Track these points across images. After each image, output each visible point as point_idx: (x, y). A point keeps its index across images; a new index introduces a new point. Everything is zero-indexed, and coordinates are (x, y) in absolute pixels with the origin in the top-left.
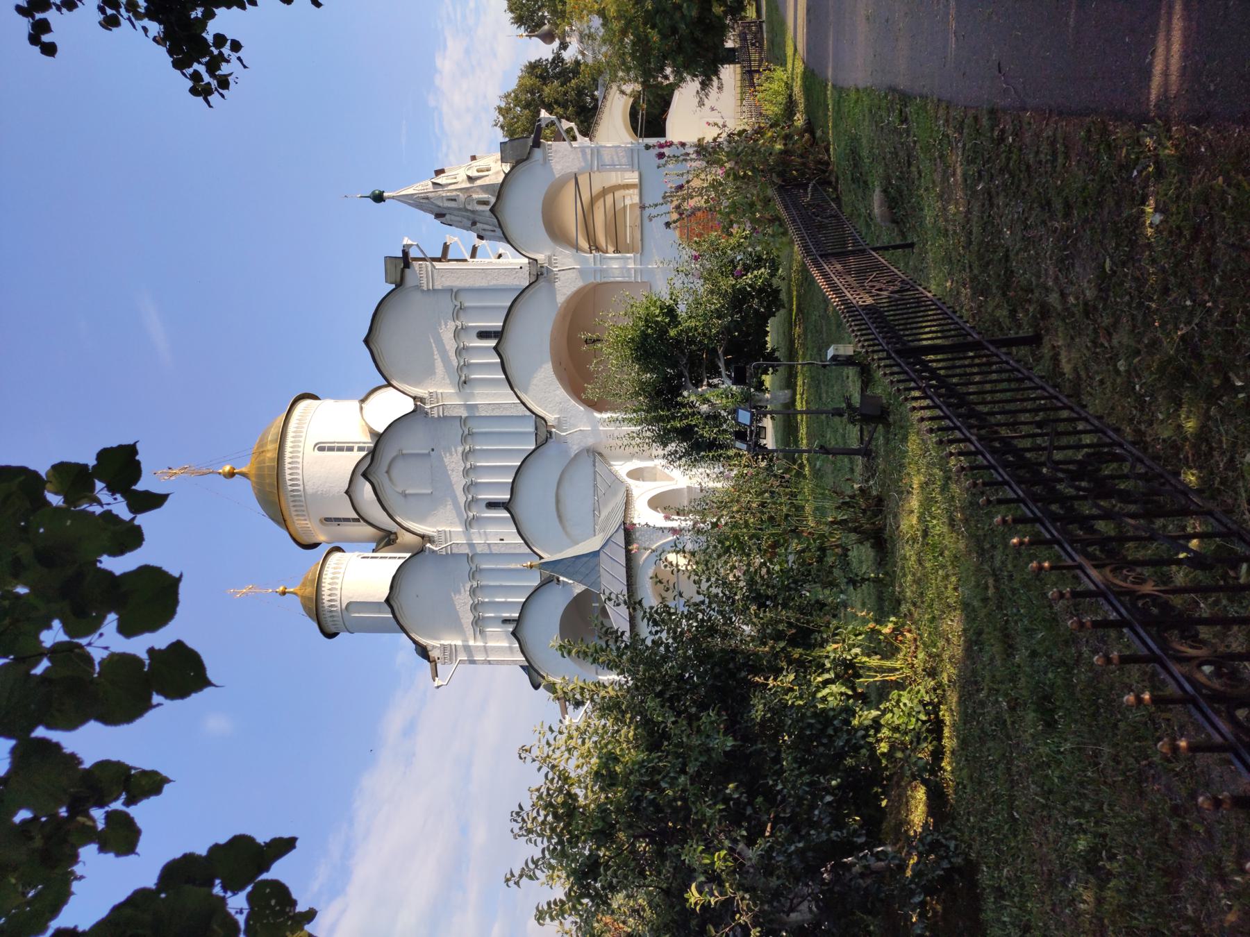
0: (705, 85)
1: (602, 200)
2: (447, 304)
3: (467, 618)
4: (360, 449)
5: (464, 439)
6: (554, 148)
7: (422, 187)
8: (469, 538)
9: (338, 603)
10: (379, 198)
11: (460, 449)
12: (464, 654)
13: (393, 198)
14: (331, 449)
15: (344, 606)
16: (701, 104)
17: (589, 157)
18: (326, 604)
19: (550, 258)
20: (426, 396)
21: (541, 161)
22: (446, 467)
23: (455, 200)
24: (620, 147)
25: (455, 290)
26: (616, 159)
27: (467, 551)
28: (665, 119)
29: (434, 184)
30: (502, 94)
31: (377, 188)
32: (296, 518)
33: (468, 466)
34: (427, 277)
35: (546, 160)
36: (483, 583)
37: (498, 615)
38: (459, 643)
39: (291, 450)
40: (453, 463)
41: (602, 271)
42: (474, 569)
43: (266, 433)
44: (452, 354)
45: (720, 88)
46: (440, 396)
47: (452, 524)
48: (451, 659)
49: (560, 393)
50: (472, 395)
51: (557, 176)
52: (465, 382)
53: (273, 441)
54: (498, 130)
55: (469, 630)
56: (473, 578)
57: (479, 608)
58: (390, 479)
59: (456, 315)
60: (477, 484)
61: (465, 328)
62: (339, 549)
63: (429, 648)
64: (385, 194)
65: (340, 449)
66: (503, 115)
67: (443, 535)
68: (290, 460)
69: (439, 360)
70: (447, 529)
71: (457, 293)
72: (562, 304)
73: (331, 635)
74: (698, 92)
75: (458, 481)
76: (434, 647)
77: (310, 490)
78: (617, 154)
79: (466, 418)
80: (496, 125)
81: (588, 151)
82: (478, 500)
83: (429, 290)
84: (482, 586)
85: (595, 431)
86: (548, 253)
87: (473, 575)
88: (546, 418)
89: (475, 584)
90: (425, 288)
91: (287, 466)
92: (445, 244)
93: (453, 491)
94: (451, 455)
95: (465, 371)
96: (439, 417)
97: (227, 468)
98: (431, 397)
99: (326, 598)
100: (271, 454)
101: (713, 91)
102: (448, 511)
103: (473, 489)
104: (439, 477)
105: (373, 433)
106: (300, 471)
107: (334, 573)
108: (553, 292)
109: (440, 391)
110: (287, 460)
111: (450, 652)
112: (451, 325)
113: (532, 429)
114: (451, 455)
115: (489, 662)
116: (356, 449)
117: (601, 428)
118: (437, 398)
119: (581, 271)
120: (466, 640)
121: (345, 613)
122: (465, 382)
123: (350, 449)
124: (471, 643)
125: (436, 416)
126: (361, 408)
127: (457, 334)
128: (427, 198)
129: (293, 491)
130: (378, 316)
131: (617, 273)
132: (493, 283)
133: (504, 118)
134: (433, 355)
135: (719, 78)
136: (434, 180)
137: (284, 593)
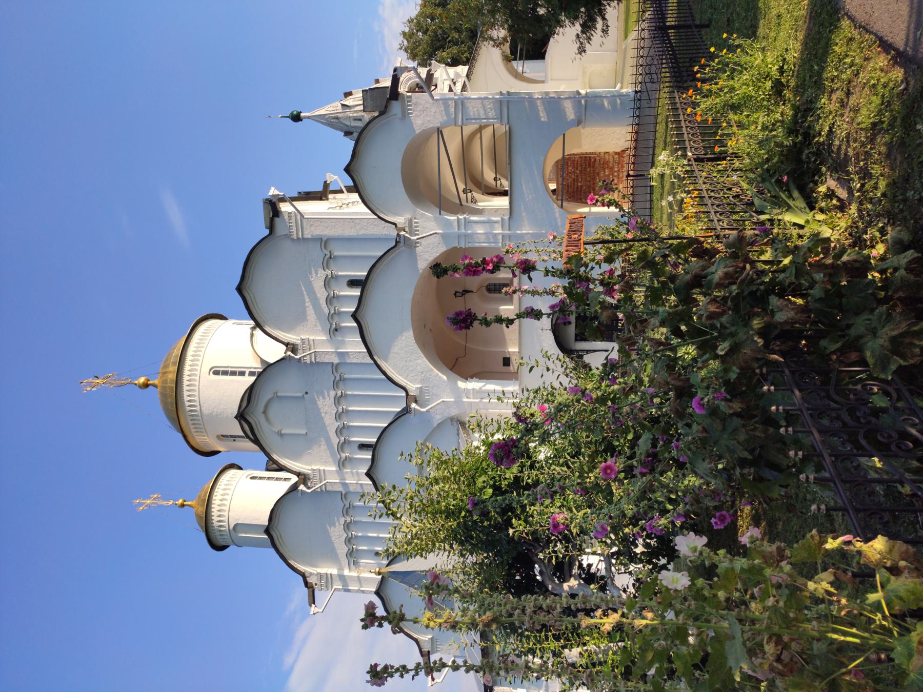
0: (588, 27)
1: (479, 134)
2: (317, 253)
3: (342, 550)
4: (252, 374)
5: (336, 385)
6: (414, 100)
7: (331, 108)
8: (343, 478)
9: (225, 524)
10: (296, 118)
11: (332, 393)
12: (339, 583)
13: (309, 117)
14: (225, 373)
15: (231, 527)
16: (582, 50)
17: (452, 110)
18: (216, 524)
19: (410, 221)
20: (298, 342)
21: (399, 115)
22: (319, 410)
23: (360, 120)
24: (486, 98)
25: (324, 239)
26: (482, 112)
27: (341, 489)
28: (545, 51)
29: (343, 105)
30: (405, 20)
31: (295, 109)
32: (195, 434)
33: (340, 410)
34: (297, 226)
35: (405, 114)
36: (357, 519)
37: (371, 548)
38: (334, 571)
39: (189, 373)
40: (326, 406)
41: (466, 236)
42: (347, 506)
43: (170, 354)
44: (323, 302)
45: (605, 31)
46: (312, 343)
47: (326, 463)
48: (327, 587)
49: (422, 362)
50: (343, 343)
51: (418, 132)
52: (336, 330)
53: (174, 363)
54: (403, 53)
55: (344, 561)
56: (347, 513)
57: (353, 541)
58: (267, 419)
59: (326, 265)
60: (349, 427)
61: (334, 278)
62: (232, 466)
63: (307, 575)
64: (302, 115)
65: (233, 373)
66: (407, 40)
67: (317, 473)
68: (188, 383)
69: (311, 307)
70: (322, 468)
71: (326, 242)
72: (424, 270)
73: (221, 548)
74: (578, 35)
75: (332, 425)
76: (311, 574)
77: (206, 411)
78: (484, 106)
79: (338, 364)
80: (401, 49)
81: (452, 104)
82: (350, 442)
83: (298, 239)
84: (355, 522)
85: (458, 402)
86: (408, 216)
87: (346, 511)
88: (408, 387)
89: (348, 520)
90: (295, 237)
91: (185, 388)
92: (325, 182)
93: (327, 432)
94: (324, 398)
95: (336, 319)
96: (311, 362)
97: (142, 380)
98: (304, 343)
99: (215, 519)
100: (172, 376)
101: (597, 35)
102: (322, 449)
103: (345, 432)
104: (314, 419)
105: (263, 361)
106: (196, 393)
107: (224, 490)
108: (413, 257)
109: (311, 338)
110: (186, 378)
111: (328, 580)
112: (322, 274)
113: (370, 457)
114: (324, 398)
115: (363, 592)
116: (247, 374)
117: (465, 400)
118: (309, 344)
119: (444, 236)
120: (341, 569)
121: (233, 533)
122: (336, 330)
123: (242, 374)
124: (346, 572)
125: (308, 362)
126: (252, 335)
127: (327, 283)
128: (337, 118)
129: (191, 411)
130: (250, 264)
131: (483, 238)
132: (362, 232)
133: (408, 41)
134: (304, 302)
135: (604, 19)
136: (342, 102)
137: (183, 505)
